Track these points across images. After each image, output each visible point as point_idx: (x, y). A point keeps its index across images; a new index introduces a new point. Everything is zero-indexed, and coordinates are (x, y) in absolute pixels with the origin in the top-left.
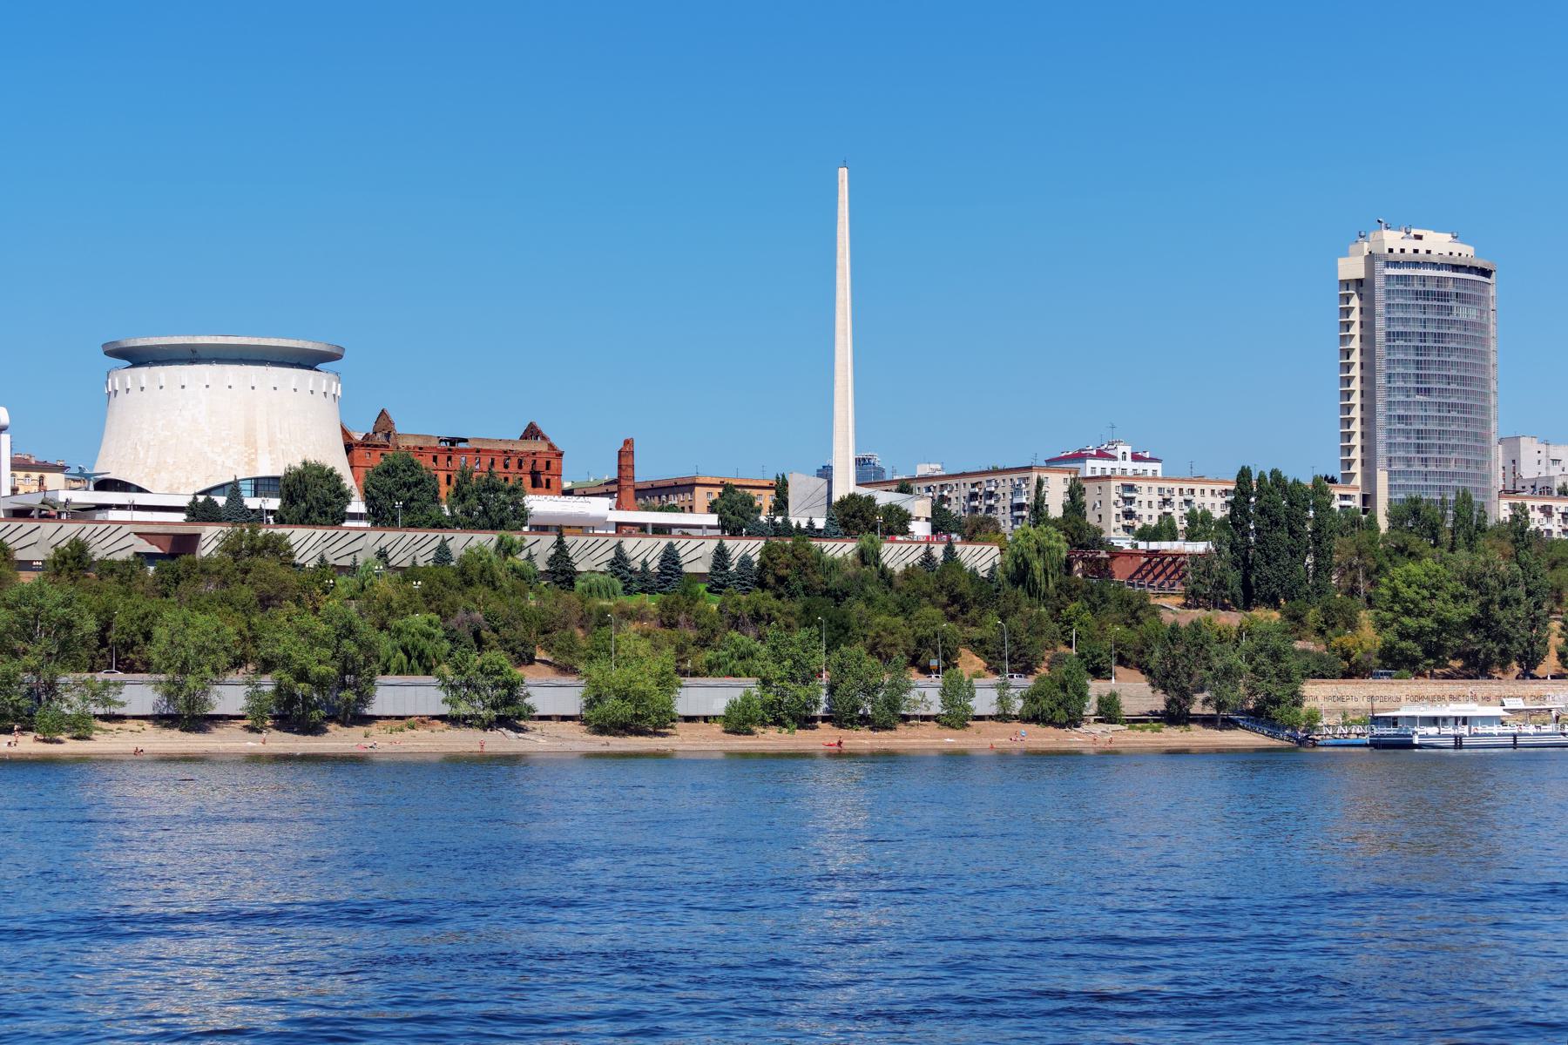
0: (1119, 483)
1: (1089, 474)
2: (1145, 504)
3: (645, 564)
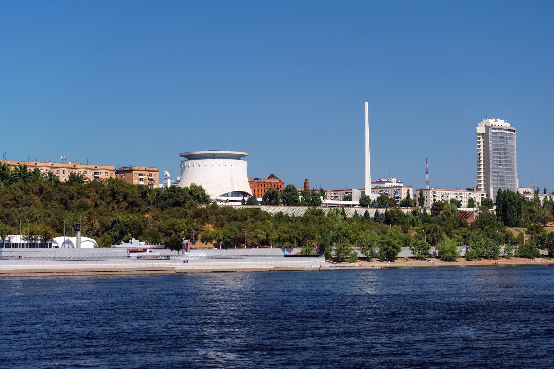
1: (386, 186)
2: (438, 197)
3: (361, 215)
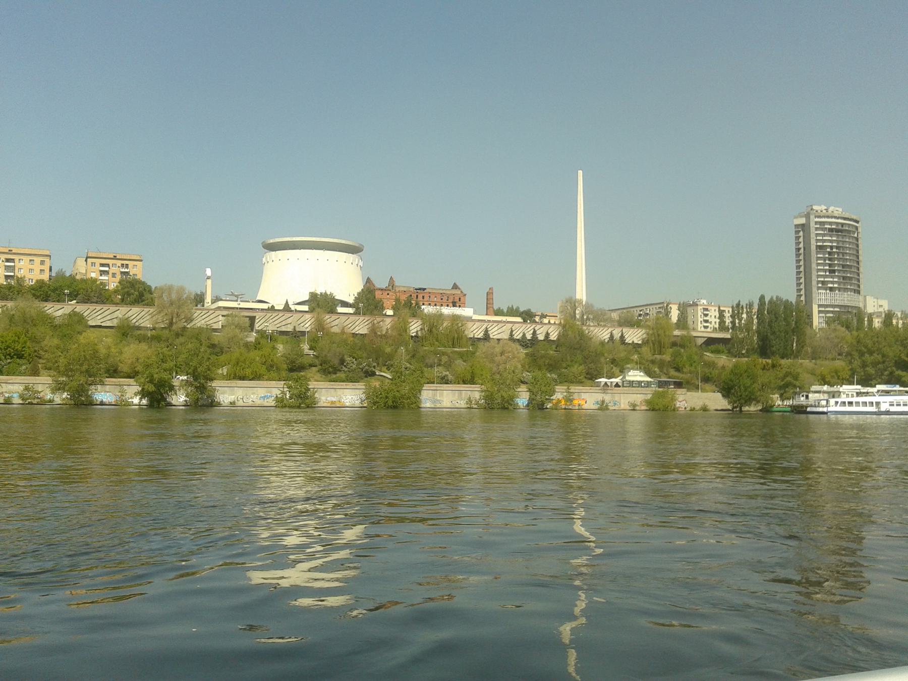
0: (702, 307)
2: (713, 317)
